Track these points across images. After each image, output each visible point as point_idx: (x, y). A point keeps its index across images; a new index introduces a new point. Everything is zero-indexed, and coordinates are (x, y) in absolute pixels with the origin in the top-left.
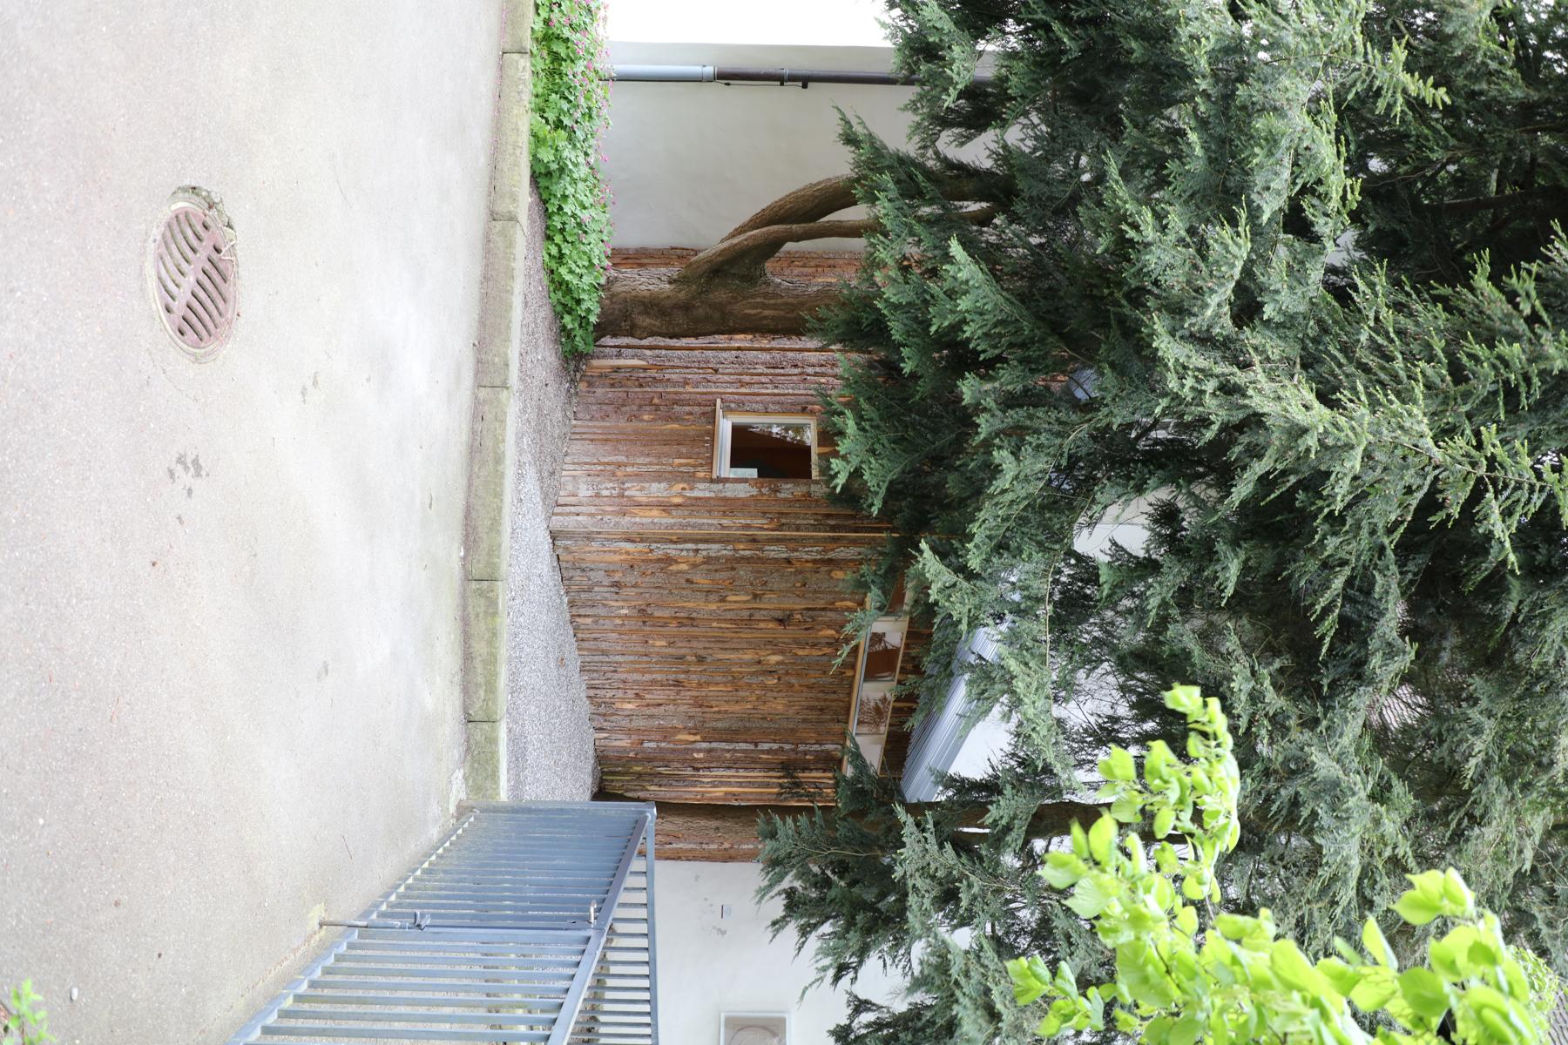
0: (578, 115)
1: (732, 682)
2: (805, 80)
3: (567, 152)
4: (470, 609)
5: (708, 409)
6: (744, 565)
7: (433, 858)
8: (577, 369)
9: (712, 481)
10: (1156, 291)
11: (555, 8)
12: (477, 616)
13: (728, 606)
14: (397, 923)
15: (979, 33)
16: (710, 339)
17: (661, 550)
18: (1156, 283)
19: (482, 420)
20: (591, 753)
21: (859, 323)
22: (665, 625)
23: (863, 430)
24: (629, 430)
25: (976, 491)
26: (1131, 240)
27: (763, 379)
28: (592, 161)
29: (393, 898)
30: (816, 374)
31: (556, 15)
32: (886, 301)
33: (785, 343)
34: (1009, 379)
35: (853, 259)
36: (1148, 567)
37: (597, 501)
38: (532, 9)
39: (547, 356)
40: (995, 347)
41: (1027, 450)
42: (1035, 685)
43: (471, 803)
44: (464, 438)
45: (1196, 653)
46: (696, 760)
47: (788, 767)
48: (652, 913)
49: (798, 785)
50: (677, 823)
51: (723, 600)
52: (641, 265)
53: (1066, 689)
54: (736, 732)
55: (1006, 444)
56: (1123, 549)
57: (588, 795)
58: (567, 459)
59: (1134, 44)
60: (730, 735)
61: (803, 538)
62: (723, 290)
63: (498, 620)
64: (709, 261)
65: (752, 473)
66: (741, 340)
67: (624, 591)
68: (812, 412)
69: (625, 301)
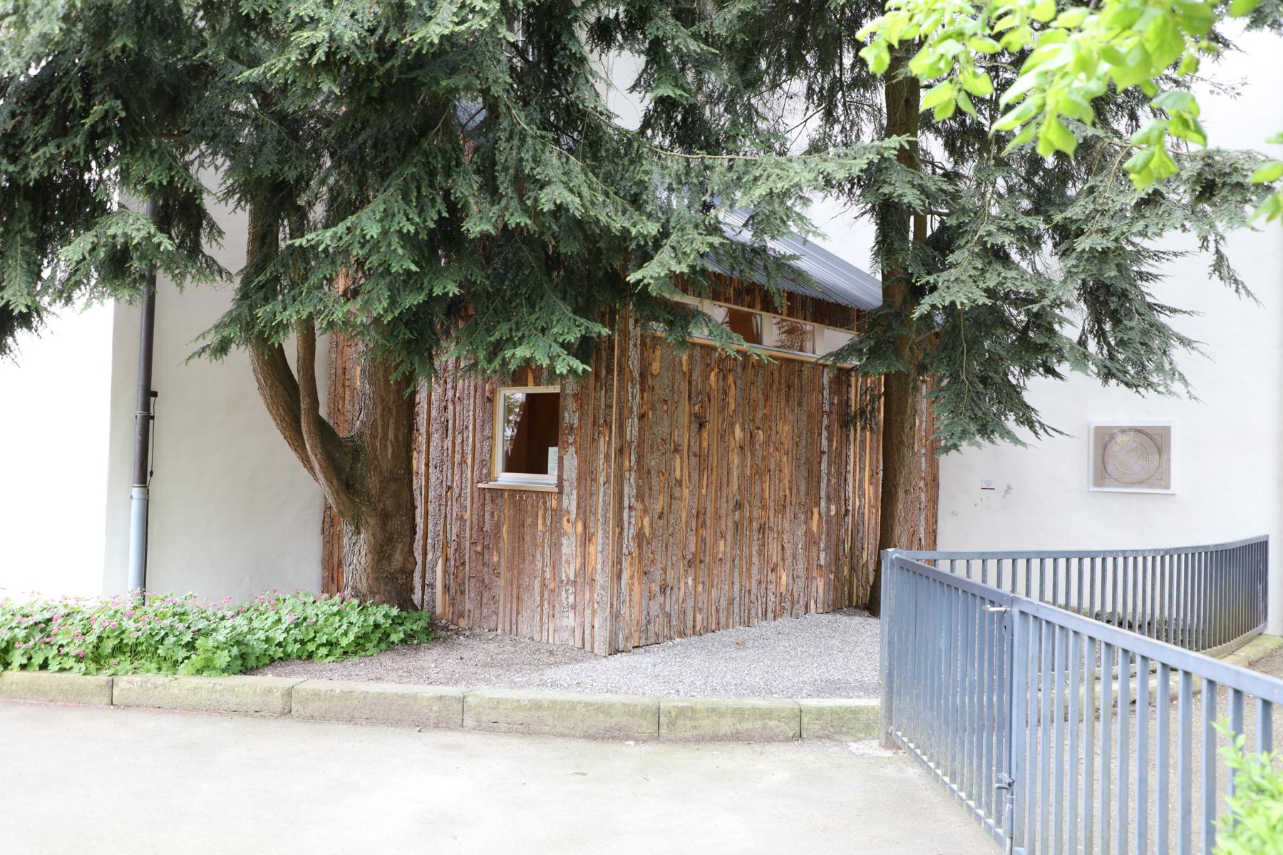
0: (181, 626)
1: (761, 475)
2: (149, 394)
3: (220, 637)
4: (687, 735)
5: (488, 496)
6: (644, 462)
7: (939, 772)
8: (446, 628)
9: (561, 492)
10: (380, 31)
11: (64, 651)
12: (695, 727)
13: (686, 477)
14: (1007, 807)
15: (100, 209)
16: (417, 493)
17: (629, 544)
18: (372, 31)
19: (497, 723)
20: (830, 617)
21: (409, 342)
22: (703, 540)
23: (521, 339)
24: (508, 576)
25: (580, 226)
26: (327, 54)
27: (458, 440)
28: (229, 614)
29: (981, 812)
30: (454, 388)
31: (73, 650)
32: (386, 311)
33: (422, 419)
34: (467, 187)
35: (336, 347)
36: (656, 53)
37: (579, 608)
38: (64, 675)
39: (431, 658)
40: (433, 201)
41: (540, 173)
42: (777, 171)
43: (882, 735)
44: (515, 741)
45: (742, 7)
46: (837, 513)
47: (846, 422)
48: (993, 555)
49: (863, 412)
50: (900, 531)
51: (679, 483)
52: (340, 564)
53: (772, 142)
54: (810, 472)
55: (532, 194)
56: (639, 80)
57: (873, 621)
58: (537, 638)
59: (119, 45)
60: (813, 478)
61: (619, 401)
62: (367, 480)
63: (699, 706)
64: (337, 493)
65: (553, 452)
66: (418, 463)
67: (670, 581)
68: (493, 392)
69: (376, 579)
